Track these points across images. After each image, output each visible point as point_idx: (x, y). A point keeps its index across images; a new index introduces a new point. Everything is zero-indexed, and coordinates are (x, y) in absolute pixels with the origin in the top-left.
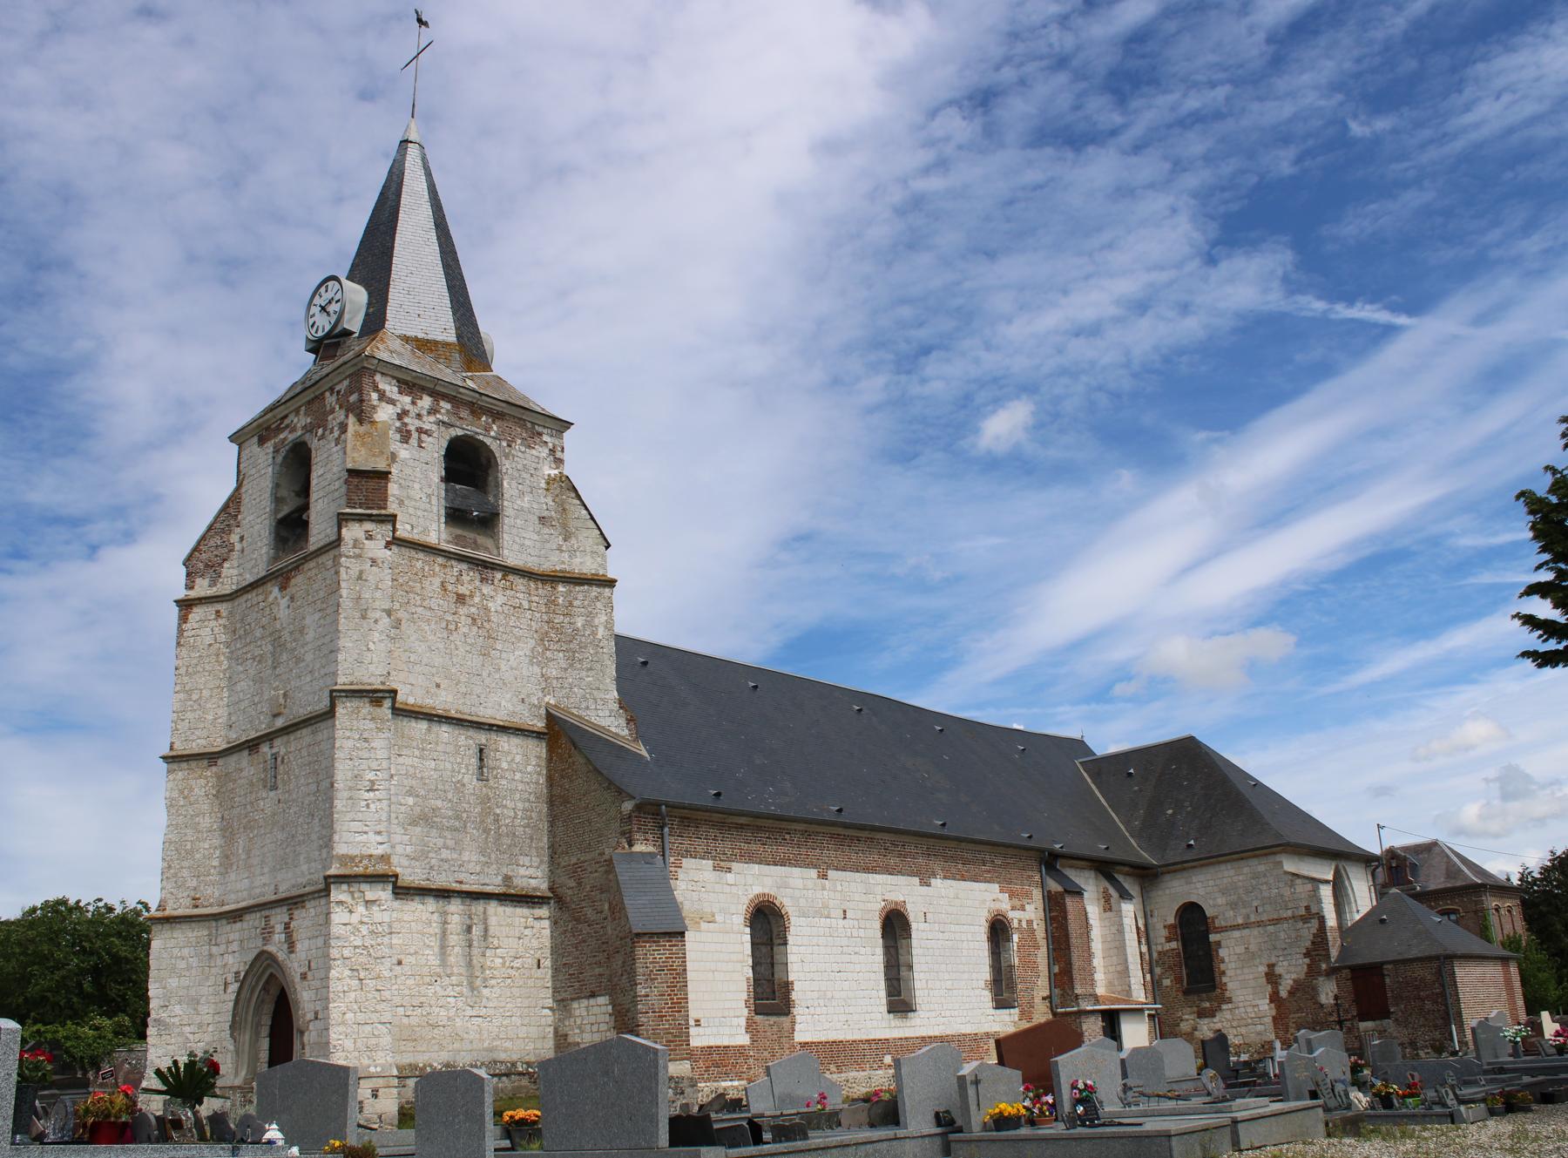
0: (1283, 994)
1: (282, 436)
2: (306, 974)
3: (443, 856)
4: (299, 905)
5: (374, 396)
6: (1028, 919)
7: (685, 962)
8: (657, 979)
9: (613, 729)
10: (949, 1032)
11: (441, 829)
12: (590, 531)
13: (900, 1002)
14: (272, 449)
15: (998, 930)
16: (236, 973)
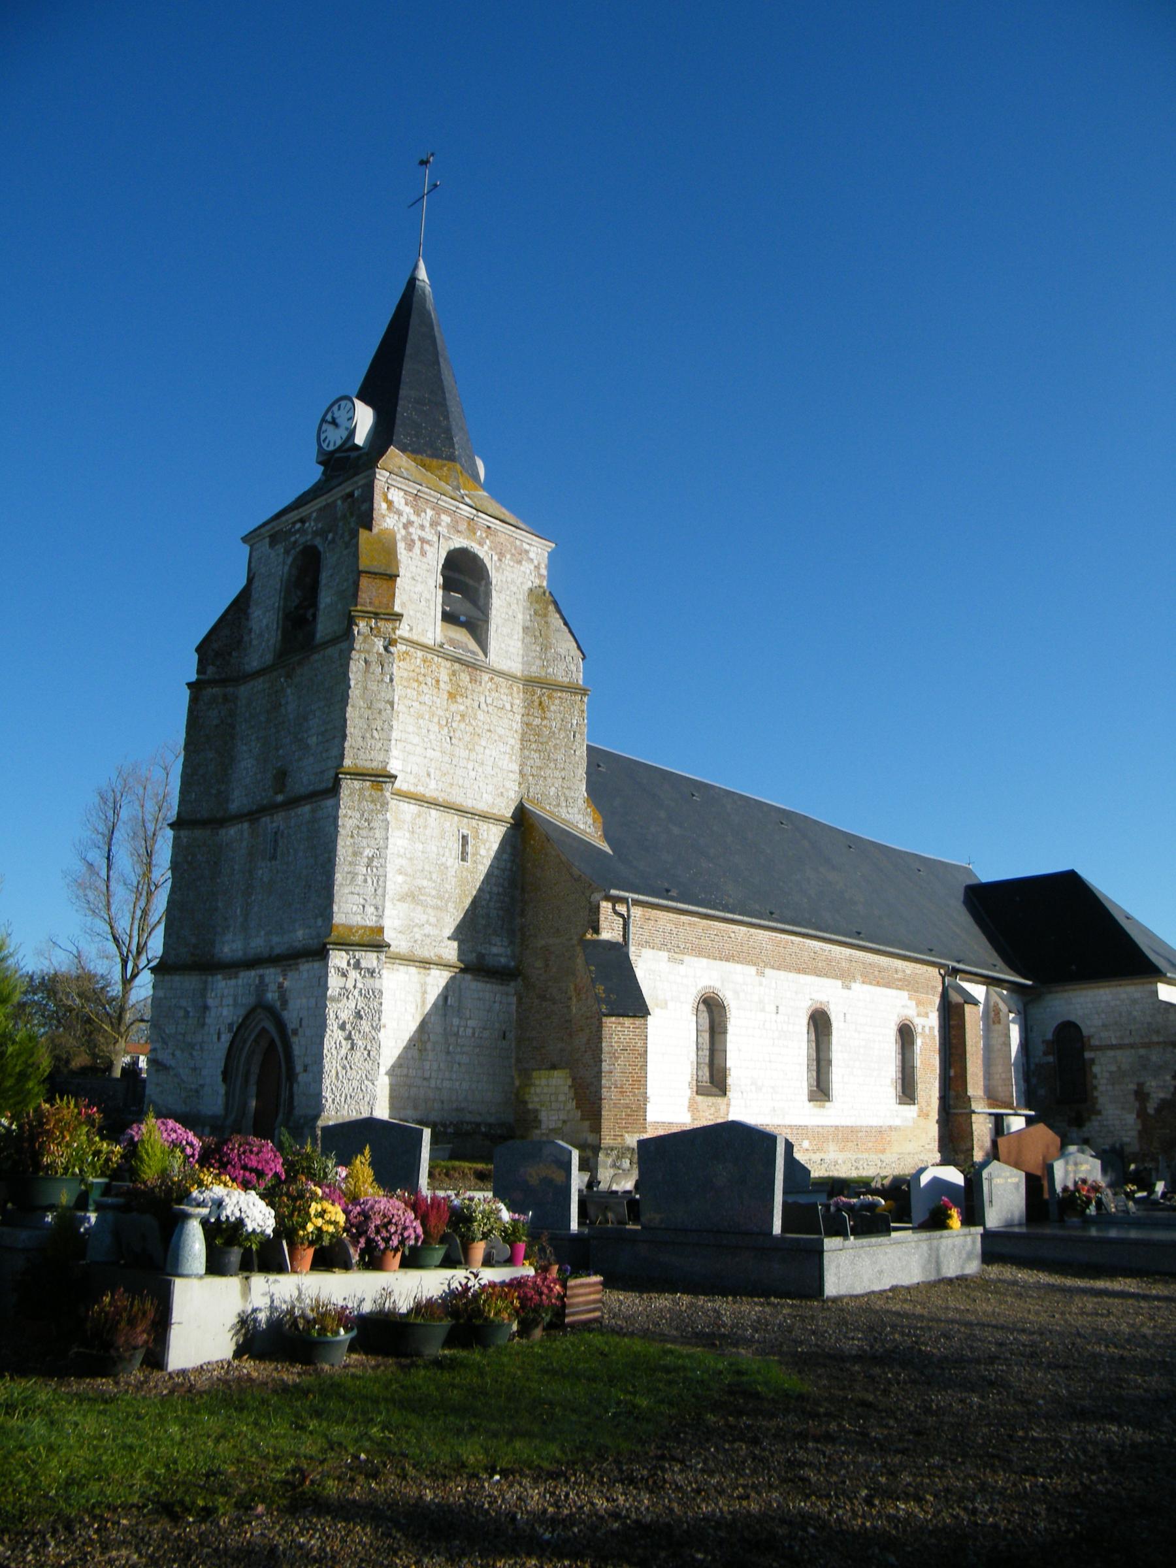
0: (1151, 1111)
1: (293, 539)
2: (297, 1030)
3: (426, 931)
4: (293, 967)
5: (384, 506)
9: (582, 826)
10: (859, 1123)
11: (425, 906)
13: (821, 1090)
14: (282, 550)
15: (906, 1034)
16: (229, 1024)
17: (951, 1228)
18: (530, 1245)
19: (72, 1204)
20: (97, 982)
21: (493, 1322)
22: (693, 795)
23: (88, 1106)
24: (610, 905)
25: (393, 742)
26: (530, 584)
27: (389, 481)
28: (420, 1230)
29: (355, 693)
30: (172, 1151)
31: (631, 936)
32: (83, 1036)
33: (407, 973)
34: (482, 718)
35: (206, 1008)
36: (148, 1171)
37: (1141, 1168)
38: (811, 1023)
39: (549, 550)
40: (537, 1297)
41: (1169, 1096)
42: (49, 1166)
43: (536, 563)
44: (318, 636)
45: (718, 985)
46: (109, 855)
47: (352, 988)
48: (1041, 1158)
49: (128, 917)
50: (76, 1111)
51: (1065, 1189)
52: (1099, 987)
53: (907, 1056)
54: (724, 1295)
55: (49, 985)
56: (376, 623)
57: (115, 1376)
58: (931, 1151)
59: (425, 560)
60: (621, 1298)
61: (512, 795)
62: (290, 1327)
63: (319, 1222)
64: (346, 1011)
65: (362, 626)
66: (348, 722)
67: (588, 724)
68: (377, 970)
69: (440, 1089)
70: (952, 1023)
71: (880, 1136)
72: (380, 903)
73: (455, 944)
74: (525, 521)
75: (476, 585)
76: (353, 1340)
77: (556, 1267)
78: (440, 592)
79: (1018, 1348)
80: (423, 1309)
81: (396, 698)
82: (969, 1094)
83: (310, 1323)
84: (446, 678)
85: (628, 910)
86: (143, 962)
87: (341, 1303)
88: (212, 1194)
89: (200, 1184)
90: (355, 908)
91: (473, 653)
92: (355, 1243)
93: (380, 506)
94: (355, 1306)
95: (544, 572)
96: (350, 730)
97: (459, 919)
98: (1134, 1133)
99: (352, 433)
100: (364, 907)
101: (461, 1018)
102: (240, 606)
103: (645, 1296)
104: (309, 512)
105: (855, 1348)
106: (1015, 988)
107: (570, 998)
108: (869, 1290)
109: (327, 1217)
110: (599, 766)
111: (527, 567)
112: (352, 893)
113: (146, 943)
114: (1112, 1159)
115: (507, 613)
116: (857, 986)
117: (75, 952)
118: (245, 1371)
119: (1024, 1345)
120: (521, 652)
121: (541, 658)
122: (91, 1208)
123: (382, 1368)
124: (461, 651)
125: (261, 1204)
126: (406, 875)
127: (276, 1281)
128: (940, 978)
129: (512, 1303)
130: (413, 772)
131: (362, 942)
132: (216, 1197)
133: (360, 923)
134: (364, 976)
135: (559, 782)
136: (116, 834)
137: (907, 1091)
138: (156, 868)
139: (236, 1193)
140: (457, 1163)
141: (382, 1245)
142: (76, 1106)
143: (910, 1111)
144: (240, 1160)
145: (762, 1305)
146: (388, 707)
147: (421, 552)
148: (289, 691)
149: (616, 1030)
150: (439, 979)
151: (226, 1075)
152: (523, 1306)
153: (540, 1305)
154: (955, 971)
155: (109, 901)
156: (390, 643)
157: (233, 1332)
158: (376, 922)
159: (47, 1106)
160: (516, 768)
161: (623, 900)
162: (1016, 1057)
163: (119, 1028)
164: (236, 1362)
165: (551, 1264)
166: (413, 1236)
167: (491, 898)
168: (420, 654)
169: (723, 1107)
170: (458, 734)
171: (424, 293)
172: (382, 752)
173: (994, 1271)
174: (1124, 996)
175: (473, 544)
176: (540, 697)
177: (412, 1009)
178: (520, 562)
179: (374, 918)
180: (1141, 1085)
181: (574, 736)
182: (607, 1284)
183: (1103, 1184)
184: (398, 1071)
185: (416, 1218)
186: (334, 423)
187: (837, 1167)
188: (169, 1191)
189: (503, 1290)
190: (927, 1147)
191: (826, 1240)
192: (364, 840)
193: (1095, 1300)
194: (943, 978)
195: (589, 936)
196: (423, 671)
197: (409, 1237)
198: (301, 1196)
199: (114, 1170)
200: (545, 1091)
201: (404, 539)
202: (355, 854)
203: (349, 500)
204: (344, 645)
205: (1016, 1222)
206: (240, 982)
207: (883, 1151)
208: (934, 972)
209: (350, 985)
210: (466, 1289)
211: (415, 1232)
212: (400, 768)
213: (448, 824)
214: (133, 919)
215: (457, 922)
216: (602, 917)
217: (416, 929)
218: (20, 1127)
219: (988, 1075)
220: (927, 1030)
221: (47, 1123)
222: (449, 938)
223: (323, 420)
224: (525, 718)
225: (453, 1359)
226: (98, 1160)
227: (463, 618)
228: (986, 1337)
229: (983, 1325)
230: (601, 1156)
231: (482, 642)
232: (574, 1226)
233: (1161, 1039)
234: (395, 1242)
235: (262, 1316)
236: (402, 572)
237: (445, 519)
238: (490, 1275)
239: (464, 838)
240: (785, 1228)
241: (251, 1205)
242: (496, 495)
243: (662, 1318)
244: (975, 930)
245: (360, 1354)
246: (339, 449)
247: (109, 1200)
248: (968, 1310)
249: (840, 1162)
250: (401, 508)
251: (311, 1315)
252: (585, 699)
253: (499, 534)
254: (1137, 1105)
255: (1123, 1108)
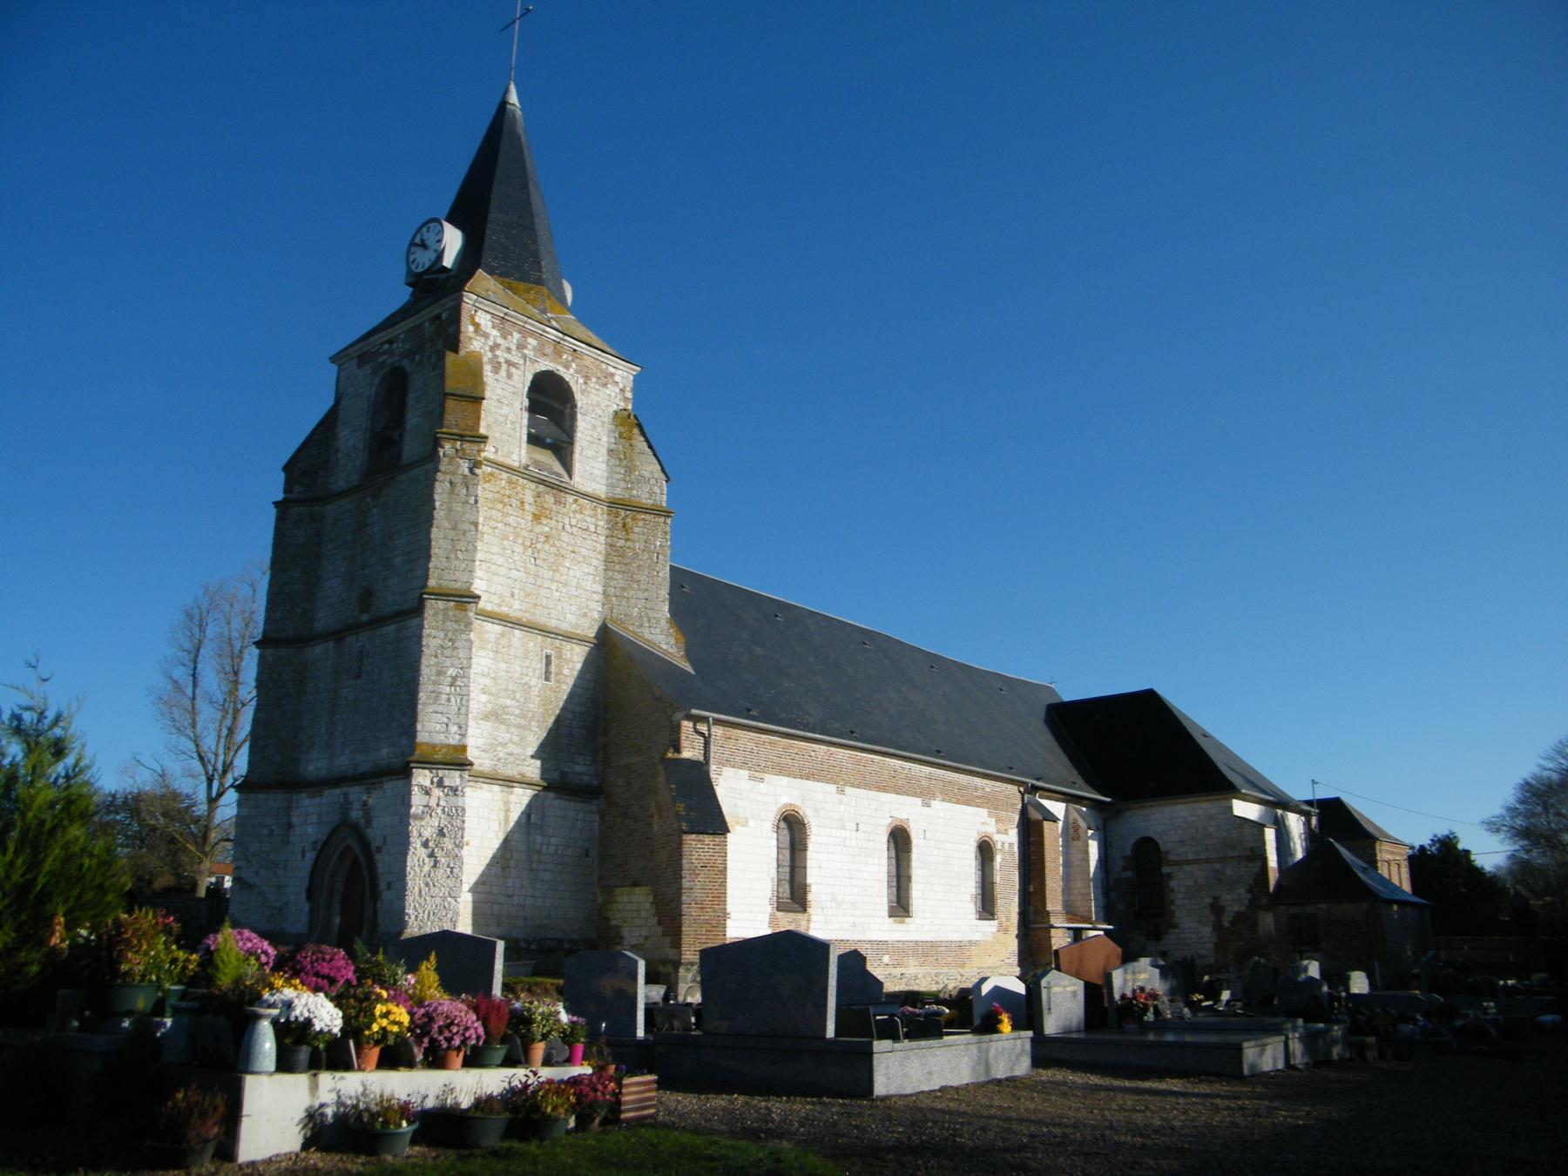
0: (1226, 924)
2: (380, 847)
3: (510, 750)
5: (471, 328)
6: (1010, 841)
7: (726, 860)
8: (700, 874)
9: (664, 647)
12: (653, 466)
13: (900, 906)
15: (985, 851)
17: (1002, 1032)
18: (588, 1045)
19: (149, 1009)
20: (182, 801)
21: (549, 1116)
22: (776, 616)
23: (164, 917)
24: (691, 724)
25: (477, 563)
26: (615, 407)
27: (477, 304)
28: (481, 1031)
29: (440, 514)
30: (247, 959)
31: (712, 755)
32: (167, 856)
33: (490, 791)
34: (566, 540)
35: (290, 826)
36: (223, 978)
37: (1214, 979)
38: (891, 841)
39: (635, 373)
40: (592, 1094)
41: (1243, 909)
42: (126, 974)
43: (621, 386)
44: (404, 456)
45: (798, 803)
46: (195, 673)
47: (435, 805)
48: (1102, 968)
49: (214, 735)
50: (154, 921)
51: (1123, 997)
52: (1175, 804)
53: (987, 872)
54: (779, 1095)
55: (133, 804)
56: (461, 445)
57: (188, 1168)
58: (1010, 965)
59: (511, 382)
60: (680, 1098)
61: (596, 615)
62: (356, 1120)
63: (384, 1022)
64: (429, 829)
65: (447, 448)
66: (433, 543)
67: (671, 546)
68: (460, 788)
69: (523, 906)
70: (1032, 839)
71: (960, 949)
72: (463, 722)
73: (538, 763)
74: (610, 345)
75: (561, 407)
76: (415, 1132)
77: (613, 1067)
78: (526, 415)
79: (1049, 1139)
80: (483, 1104)
81: (481, 520)
82: (1048, 909)
83: (374, 1116)
84: (531, 500)
85: (709, 730)
86: (229, 780)
87: (404, 1098)
88: (282, 997)
89: (271, 987)
90: (438, 727)
91: (558, 475)
92: (420, 1043)
93: (468, 329)
94: (419, 1101)
95: (629, 395)
96: (434, 551)
97: (542, 738)
98: (1210, 946)
99: (440, 255)
100: (447, 725)
101: (544, 836)
102: (328, 424)
103: (703, 1097)
104: (397, 332)
105: (894, 1140)
106: (1094, 805)
107: (652, 816)
108: (919, 1090)
109: (391, 1017)
110: (683, 587)
111: (612, 390)
112: (436, 712)
113: (232, 762)
114: (1183, 974)
115: (592, 436)
116: (936, 804)
117: (159, 770)
118: (312, 1162)
119: (1055, 1137)
120: (605, 474)
121: (625, 481)
122: (168, 1014)
123: (442, 1158)
124: (545, 473)
125: (329, 1006)
126: (490, 694)
127: (342, 1078)
128: (1019, 796)
129: (568, 1099)
130: (498, 593)
131: (444, 761)
132: (286, 999)
133: (443, 742)
134: (447, 795)
135: (641, 604)
136: (203, 651)
137: (987, 907)
138: (244, 686)
139: (305, 995)
140: (539, 979)
141: (445, 1045)
142: (155, 916)
143: (990, 927)
144: (313, 967)
145: (813, 1104)
146: (473, 528)
147: (508, 375)
148: (375, 510)
149: (696, 848)
150: (521, 798)
151: (310, 893)
152: (579, 1102)
153: (596, 1100)
154: (1035, 789)
155: (194, 720)
156: (475, 464)
157: (301, 1126)
158: (460, 741)
159: (126, 916)
160: (599, 588)
161: (704, 720)
162: (1094, 873)
163: (203, 848)
164: (303, 1155)
165: (607, 1064)
166: (474, 1036)
167: (574, 717)
168: (505, 475)
169: (804, 923)
170: (542, 555)
171: (514, 116)
172: (467, 573)
173: (1046, 1074)
174: (1199, 812)
175: (559, 368)
176: (623, 519)
177: (495, 826)
178: (605, 385)
179: (457, 737)
180: (1216, 898)
181: (657, 558)
182: (661, 1085)
183: (1160, 993)
184: (481, 888)
185: (478, 1019)
186: (424, 246)
187: (917, 981)
188: (242, 994)
189: (560, 1087)
190: (1007, 961)
191: (875, 1043)
192: (448, 660)
193: (1137, 1098)
194: (1023, 795)
195: (670, 755)
196: (508, 492)
197: (470, 1037)
198: (367, 997)
199: (191, 978)
200: (627, 907)
201: (491, 361)
202: (439, 673)
203: (437, 322)
204: (429, 467)
205: (1074, 1028)
206: (325, 800)
207: (963, 966)
208: (1013, 789)
209: (433, 803)
210: (526, 1086)
211: (476, 1032)
212: (484, 588)
213: (532, 644)
214: (219, 736)
215: (540, 741)
216: (683, 737)
217: (498, 748)
218: (99, 937)
219: (1067, 891)
220: (1006, 846)
221: (125, 932)
222: (532, 757)
223: (412, 244)
224: (609, 540)
225: (509, 1150)
226: (175, 968)
227: (548, 441)
228: (1021, 1130)
229: (1021, 1120)
230: (682, 971)
231: (567, 463)
232: (640, 1033)
233: (1236, 854)
234: (457, 1042)
235: (329, 1111)
236: (488, 394)
237: (532, 342)
238: (546, 1073)
239: (548, 657)
240: (838, 1031)
241: (319, 1006)
242: (583, 319)
243: (716, 1114)
244: (1056, 748)
245: (421, 1146)
246: (428, 271)
247: (184, 1004)
248: (1010, 1107)
249: (920, 976)
250: (488, 331)
251: (374, 1108)
252: (669, 521)
253: (586, 357)
254: (1212, 918)
255: (1199, 922)
